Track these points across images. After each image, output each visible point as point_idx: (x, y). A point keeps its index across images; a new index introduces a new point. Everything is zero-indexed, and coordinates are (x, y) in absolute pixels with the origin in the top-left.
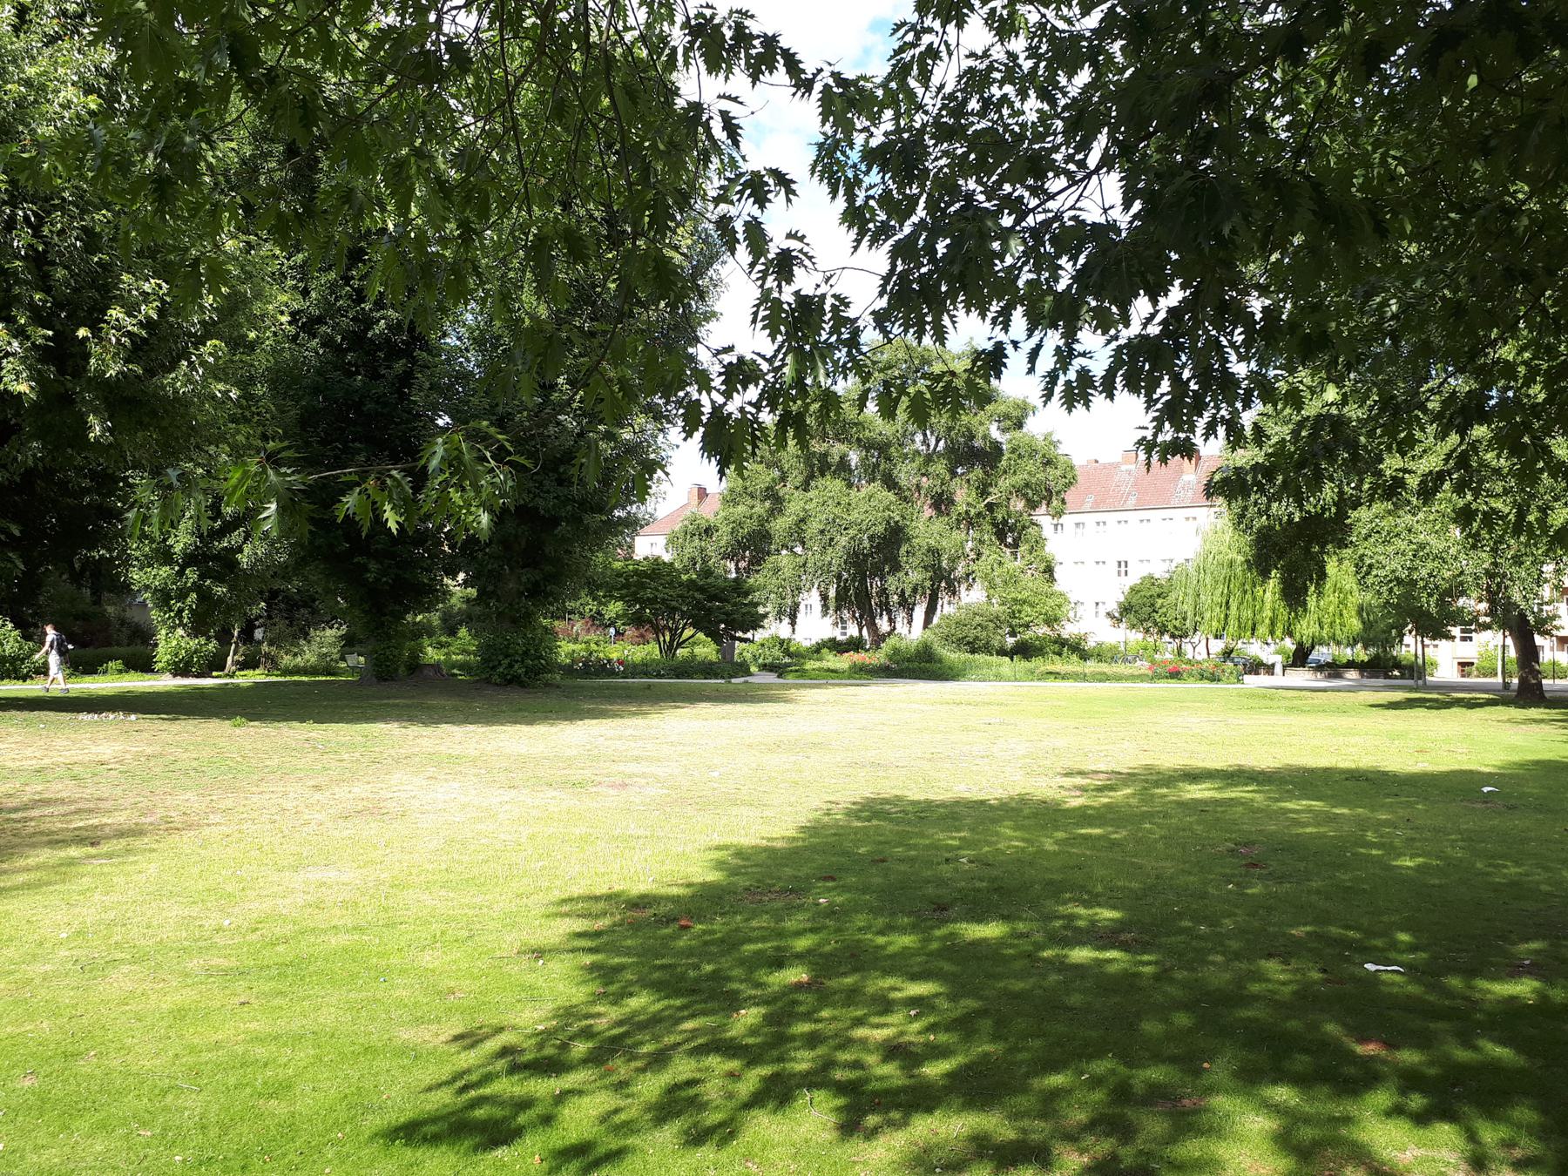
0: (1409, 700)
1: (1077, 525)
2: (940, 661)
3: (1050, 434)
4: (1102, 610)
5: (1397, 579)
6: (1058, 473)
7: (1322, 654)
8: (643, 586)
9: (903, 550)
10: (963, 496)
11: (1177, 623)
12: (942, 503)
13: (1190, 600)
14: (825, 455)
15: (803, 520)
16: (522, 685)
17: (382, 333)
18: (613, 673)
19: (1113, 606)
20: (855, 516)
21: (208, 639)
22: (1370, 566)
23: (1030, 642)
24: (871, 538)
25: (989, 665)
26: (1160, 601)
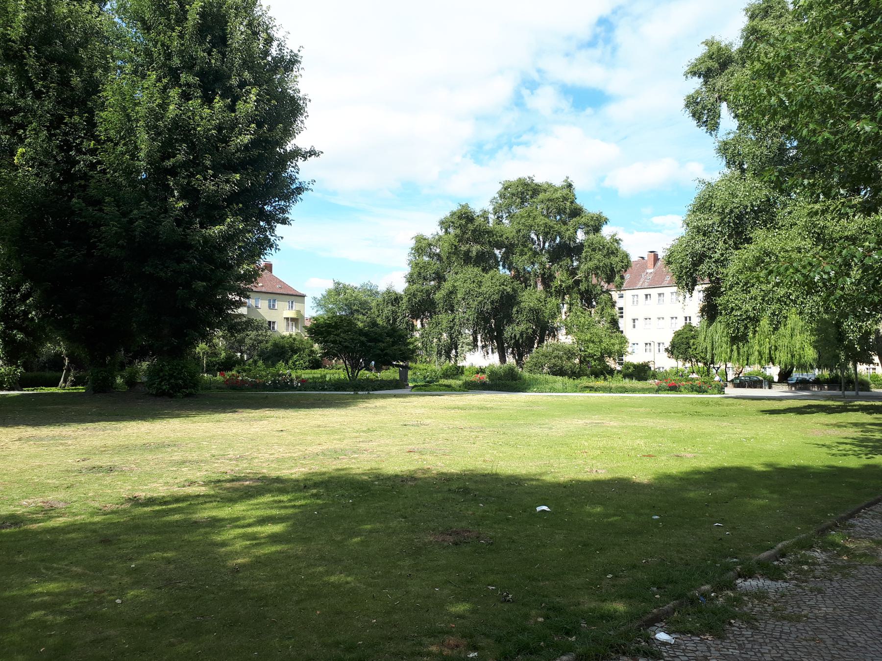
0: (810, 406)
1: (660, 295)
2: (520, 378)
3: (615, 235)
4: (662, 348)
5: (748, 317)
6: (617, 259)
7: (796, 375)
8: (329, 333)
9: (515, 309)
10: (560, 277)
11: (703, 355)
12: (547, 279)
13: (708, 340)
14: (469, 251)
15: (451, 293)
16: (171, 396)
17: (79, 171)
18: (292, 388)
19: (667, 345)
20: (483, 289)
21: (18, 367)
22: (732, 309)
23: (595, 366)
24: (492, 303)
25: (547, 382)
26: (692, 341)
